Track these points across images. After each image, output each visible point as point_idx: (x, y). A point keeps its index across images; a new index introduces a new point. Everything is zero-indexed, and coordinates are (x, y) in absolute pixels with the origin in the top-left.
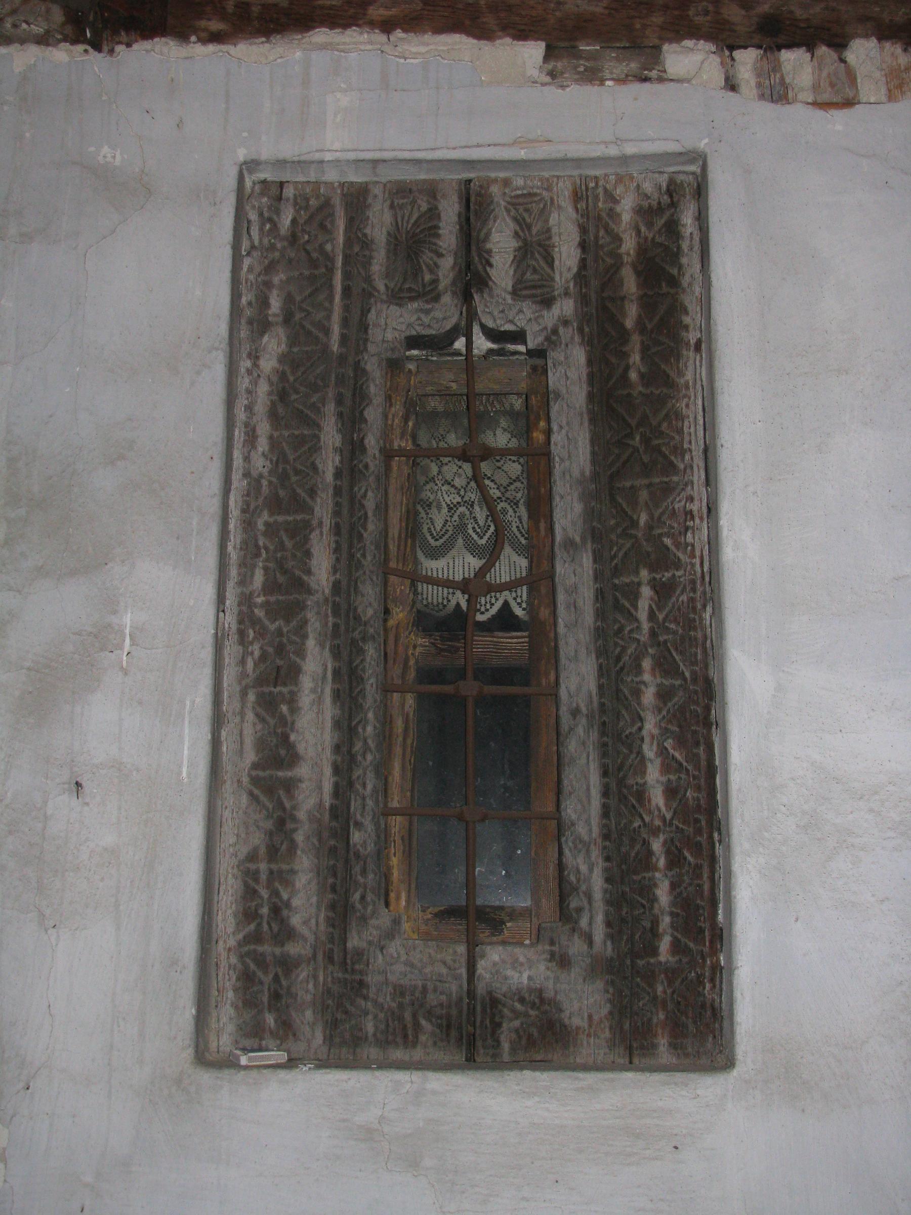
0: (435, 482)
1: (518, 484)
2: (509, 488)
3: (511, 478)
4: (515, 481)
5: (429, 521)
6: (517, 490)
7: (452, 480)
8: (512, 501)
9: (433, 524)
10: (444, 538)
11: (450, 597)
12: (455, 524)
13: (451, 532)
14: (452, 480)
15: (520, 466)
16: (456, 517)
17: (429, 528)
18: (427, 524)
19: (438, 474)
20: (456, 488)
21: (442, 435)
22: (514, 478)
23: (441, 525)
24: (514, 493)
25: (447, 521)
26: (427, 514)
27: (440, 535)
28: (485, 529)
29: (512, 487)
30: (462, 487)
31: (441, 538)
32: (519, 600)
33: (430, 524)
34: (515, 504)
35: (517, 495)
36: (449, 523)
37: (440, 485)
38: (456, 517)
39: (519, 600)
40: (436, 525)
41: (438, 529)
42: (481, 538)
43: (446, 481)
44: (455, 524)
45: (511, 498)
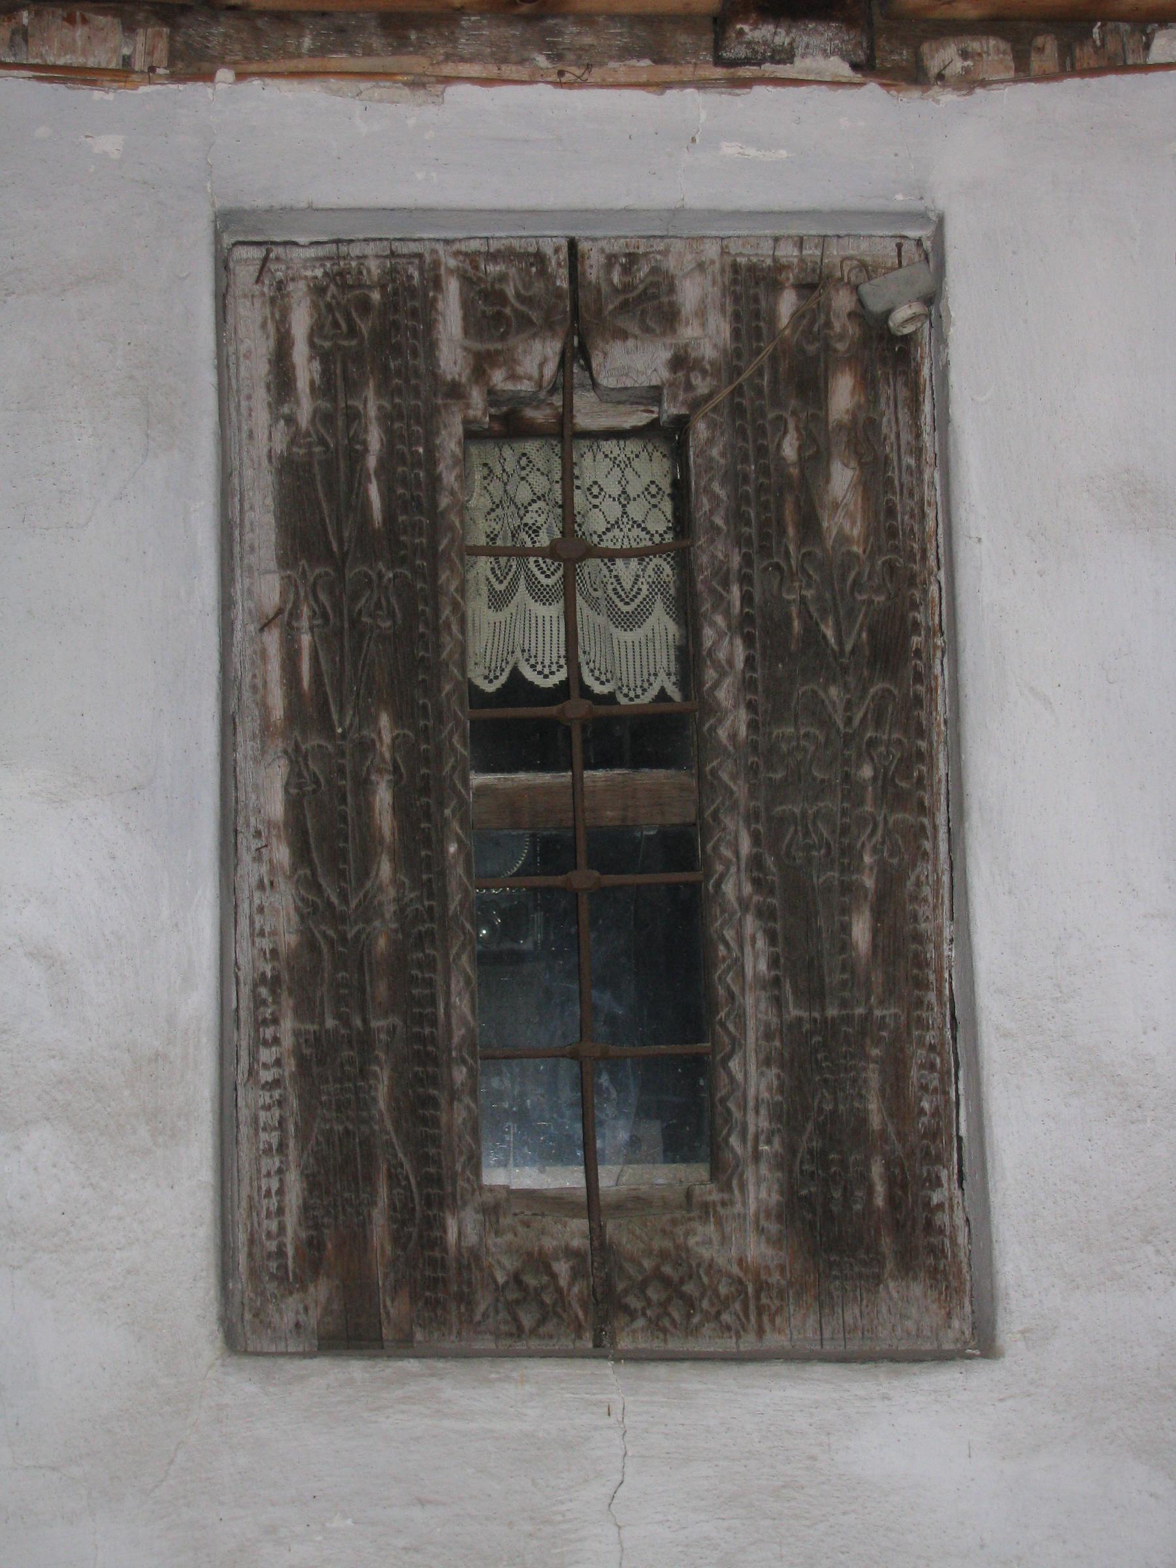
0: (618, 527)
1: (541, 504)
2: (530, 508)
3: (535, 494)
4: (539, 498)
5: (613, 580)
6: (540, 512)
7: (643, 522)
8: (530, 528)
9: (620, 584)
10: (637, 601)
11: (652, 678)
12: (650, 580)
13: (644, 592)
14: (643, 522)
15: (547, 483)
16: (649, 571)
17: (615, 589)
18: (612, 583)
19: (622, 516)
20: (648, 533)
21: (629, 459)
22: (539, 494)
23: (631, 583)
24: (536, 515)
25: (638, 576)
26: (611, 571)
27: (631, 596)
28: (506, 570)
29: (535, 506)
30: (657, 532)
31: (632, 600)
32: (532, 661)
33: (615, 584)
34: (534, 531)
35: (539, 519)
36: (641, 580)
37: (626, 530)
38: (649, 571)
39: (532, 661)
40: (624, 584)
41: (627, 587)
42: (501, 582)
43: (635, 522)
44: (650, 580)
45: (530, 522)
